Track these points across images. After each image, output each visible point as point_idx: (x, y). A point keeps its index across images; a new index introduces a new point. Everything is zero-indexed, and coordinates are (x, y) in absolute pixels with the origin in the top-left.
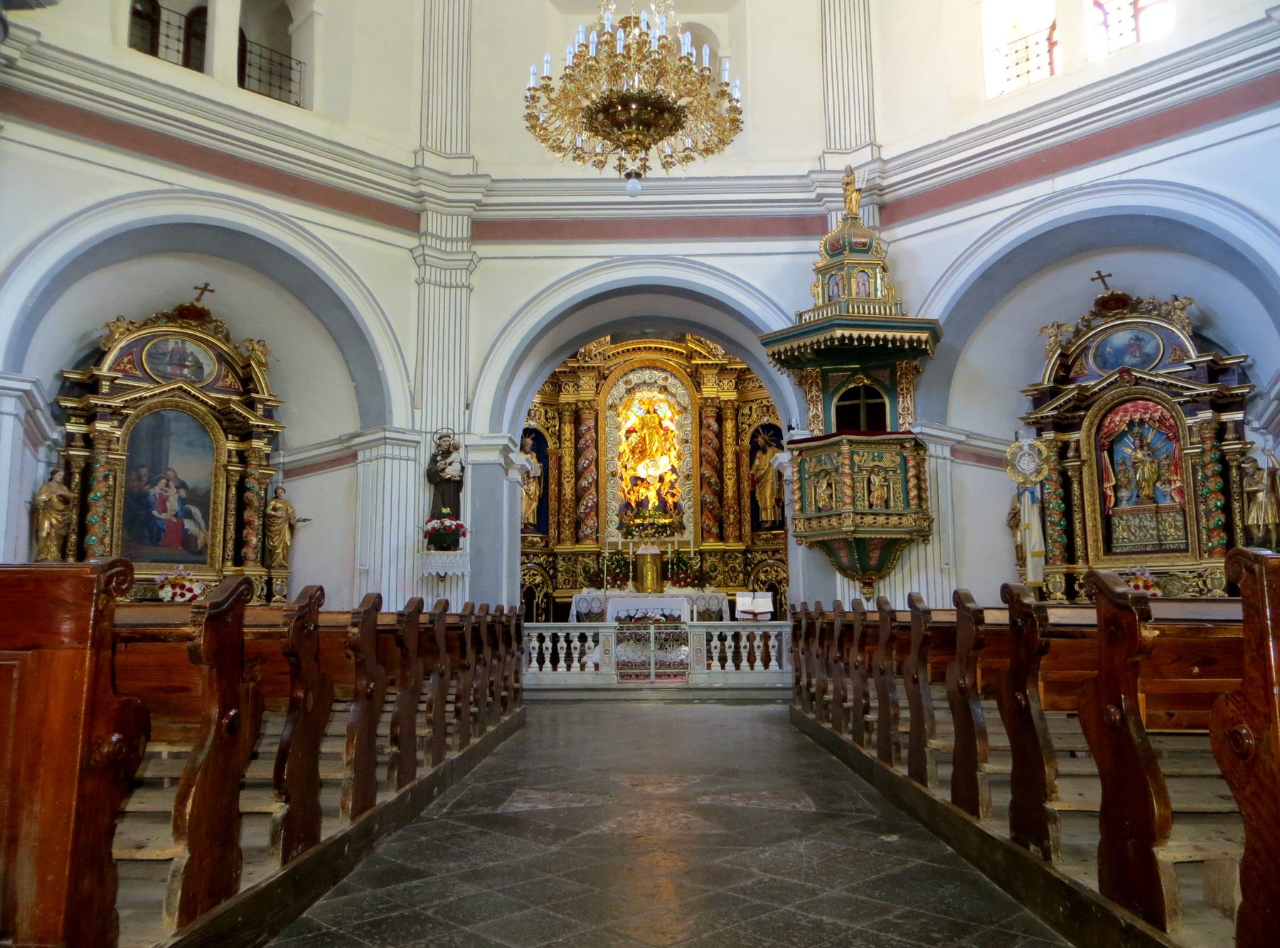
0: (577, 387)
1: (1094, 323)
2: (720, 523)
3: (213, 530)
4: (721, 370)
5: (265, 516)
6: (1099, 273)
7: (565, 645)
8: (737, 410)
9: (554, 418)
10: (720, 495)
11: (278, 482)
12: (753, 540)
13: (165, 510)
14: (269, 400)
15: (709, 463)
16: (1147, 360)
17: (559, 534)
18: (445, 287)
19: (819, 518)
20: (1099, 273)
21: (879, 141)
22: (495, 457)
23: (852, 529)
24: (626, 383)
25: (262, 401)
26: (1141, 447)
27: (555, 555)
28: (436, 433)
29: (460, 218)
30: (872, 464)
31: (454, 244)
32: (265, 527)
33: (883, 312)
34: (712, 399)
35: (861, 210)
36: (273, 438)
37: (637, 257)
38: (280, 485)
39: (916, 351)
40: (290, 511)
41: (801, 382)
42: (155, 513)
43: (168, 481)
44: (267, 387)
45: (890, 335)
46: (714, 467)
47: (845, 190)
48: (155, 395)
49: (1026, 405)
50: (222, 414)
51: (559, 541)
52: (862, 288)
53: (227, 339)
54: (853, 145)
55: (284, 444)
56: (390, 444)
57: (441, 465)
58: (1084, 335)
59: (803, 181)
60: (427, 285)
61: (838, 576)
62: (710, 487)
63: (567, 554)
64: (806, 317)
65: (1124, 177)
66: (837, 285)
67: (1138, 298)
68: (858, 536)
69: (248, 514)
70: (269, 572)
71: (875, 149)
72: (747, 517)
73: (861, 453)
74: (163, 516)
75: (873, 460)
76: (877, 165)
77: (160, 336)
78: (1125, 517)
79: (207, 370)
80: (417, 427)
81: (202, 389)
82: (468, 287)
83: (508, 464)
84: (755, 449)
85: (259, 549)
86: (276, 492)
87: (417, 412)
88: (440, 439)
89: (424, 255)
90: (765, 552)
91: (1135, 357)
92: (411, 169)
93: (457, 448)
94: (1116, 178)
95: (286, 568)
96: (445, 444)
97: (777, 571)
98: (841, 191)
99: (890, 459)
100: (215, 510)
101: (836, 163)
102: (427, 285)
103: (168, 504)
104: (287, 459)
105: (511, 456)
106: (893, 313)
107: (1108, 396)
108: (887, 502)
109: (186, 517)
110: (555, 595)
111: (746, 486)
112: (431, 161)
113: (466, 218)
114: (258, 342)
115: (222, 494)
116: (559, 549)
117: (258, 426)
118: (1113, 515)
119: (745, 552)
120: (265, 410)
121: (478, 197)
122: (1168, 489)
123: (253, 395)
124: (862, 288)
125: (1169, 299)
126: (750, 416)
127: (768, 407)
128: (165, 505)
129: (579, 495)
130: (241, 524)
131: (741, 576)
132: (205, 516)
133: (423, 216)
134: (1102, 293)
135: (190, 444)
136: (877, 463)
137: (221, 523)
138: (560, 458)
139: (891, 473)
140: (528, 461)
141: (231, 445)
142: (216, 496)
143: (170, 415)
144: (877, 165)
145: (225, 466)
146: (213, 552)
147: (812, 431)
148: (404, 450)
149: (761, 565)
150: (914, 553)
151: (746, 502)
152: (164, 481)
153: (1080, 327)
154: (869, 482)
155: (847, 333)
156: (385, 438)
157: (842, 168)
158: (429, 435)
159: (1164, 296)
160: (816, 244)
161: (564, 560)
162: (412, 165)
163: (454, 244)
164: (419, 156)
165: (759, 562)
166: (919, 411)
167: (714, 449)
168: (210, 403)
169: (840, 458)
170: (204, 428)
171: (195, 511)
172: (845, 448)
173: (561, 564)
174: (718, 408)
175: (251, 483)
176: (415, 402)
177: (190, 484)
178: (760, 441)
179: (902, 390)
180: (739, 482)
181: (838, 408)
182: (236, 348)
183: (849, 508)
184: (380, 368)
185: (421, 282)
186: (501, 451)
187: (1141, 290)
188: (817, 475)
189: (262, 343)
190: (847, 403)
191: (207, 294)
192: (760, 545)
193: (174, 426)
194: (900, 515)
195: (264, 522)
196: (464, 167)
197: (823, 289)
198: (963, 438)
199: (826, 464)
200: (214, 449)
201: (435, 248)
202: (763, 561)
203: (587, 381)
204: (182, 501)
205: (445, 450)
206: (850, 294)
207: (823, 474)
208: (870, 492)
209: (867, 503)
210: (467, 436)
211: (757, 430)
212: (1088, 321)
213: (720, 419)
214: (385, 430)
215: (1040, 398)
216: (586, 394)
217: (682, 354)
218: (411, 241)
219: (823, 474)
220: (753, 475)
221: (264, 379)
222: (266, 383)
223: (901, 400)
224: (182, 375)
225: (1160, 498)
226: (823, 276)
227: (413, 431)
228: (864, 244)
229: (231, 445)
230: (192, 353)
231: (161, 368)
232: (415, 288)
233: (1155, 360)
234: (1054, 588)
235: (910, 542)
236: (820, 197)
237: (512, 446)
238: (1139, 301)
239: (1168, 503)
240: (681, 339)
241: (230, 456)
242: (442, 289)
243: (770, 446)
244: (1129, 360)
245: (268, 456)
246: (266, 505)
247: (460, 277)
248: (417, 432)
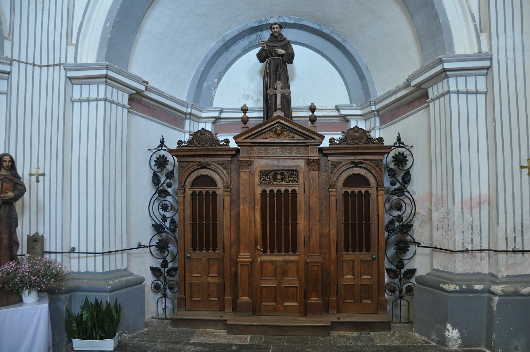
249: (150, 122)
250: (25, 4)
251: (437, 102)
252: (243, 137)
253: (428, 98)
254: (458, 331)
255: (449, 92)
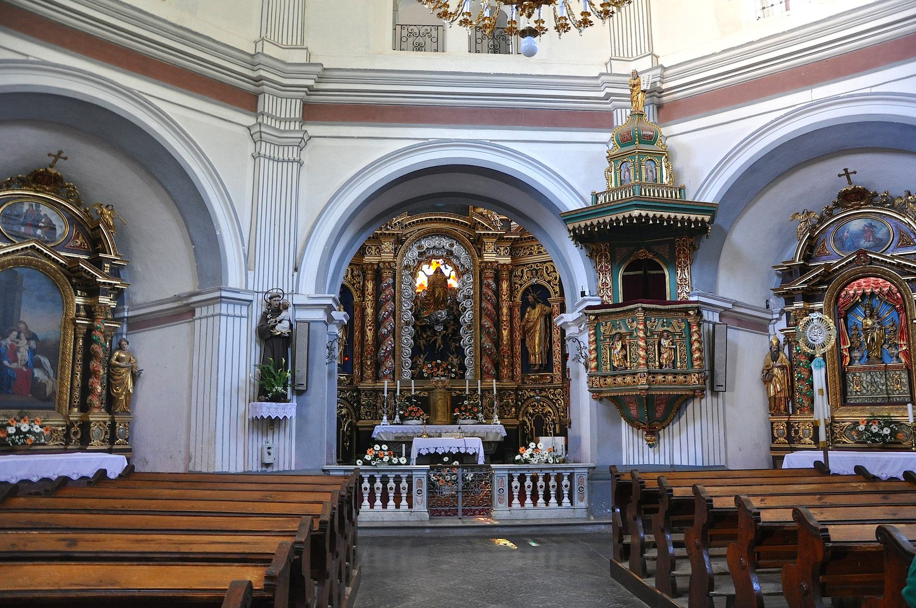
0: (379, 251)
1: (835, 211)
2: (497, 365)
3: (62, 379)
4: (499, 239)
5: (110, 366)
6: (846, 170)
7: (394, 485)
8: (511, 272)
9: (359, 276)
10: (497, 342)
11: (122, 334)
12: (523, 379)
13: (15, 360)
14: (115, 260)
15: (489, 316)
16: (880, 244)
17: (362, 374)
18: (278, 161)
19: (614, 376)
20: (846, 170)
21: (655, 52)
22: (320, 315)
23: (647, 387)
24: (420, 247)
25: (109, 261)
26: (871, 316)
27: (358, 391)
28: (267, 293)
29: (294, 101)
30: (661, 329)
31: (288, 124)
32: (110, 376)
33: (661, 195)
34: (491, 263)
35: (647, 108)
36: (119, 294)
37: (450, 140)
38: (124, 337)
39: (701, 230)
40: (133, 361)
41: (592, 255)
42: (6, 363)
43: (19, 333)
44: (113, 248)
45: (665, 215)
46: (492, 320)
47: (632, 91)
48: (8, 253)
49: (776, 281)
50: (72, 272)
51: (362, 379)
52: (650, 174)
53: (78, 204)
54: (635, 54)
55: (129, 298)
56: (225, 302)
57: (271, 322)
58: (826, 221)
59: (593, 82)
60: (262, 159)
61: (624, 425)
62: (489, 336)
63: (369, 390)
64: (601, 199)
65: (874, 90)
66: (628, 170)
67: (875, 193)
68: (650, 393)
69: (94, 364)
70: (113, 418)
71: (655, 58)
72: (518, 361)
73: (653, 319)
74: (14, 365)
75: (663, 326)
76: (659, 71)
77: (15, 199)
78: (858, 374)
79: (59, 231)
80: (250, 288)
81: (51, 249)
82: (298, 162)
83: (331, 319)
84: (526, 304)
85: (104, 396)
86: (120, 344)
87: (251, 274)
88: (270, 298)
89: (261, 132)
90: (533, 390)
91: (869, 241)
92: (252, 56)
93: (286, 308)
94: (868, 91)
95: (129, 413)
96: (275, 303)
97: (543, 406)
98: (629, 92)
99: (676, 325)
100: (63, 360)
101: (625, 68)
102: (262, 159)
103: (19, 355)
104: (131, 314)
105: (333, 313)
106: (674, 195)
107: (845, 272)
108: (674, 362)
109: (35, 367)
110: (358, 424)
111: (518, 336)
112: (270, 50)
113: (298, 101)
114: (107, 207)
115: (70, 345)
116: (362, 386)
117: (104, 283)
118: (848, 372)
119: (516, 390)
120: (111, 268)
121: (311, 82)
122: (895, 351)
123: (101, 255)
124: (650, 174)
125: (903, 195)
126: (522, 277)
127: (537, 271)
128: (16, 355)
129: (378, 341)
130: (88, 373)
131: (513, 409)
132: (54, 366)
133: (261, 97)
134: (845, 187)
135: (41, 299)
136: (666, 328)
137: (68, 372)
138: (363, 309)
139: (677, 337)
140: (340, 315)
141: (79, 300)
142: (65, 347)
143: (20, 271)
144: (659, 71)
145: (73, 320)
146: (60, 399)
147: (602, 297)
148: (238, 307)
149: (530, 401)
150: (690, 407)
151: (518, 347)
152: (15, 333)
153: (824, 214)
154: (660, 344)
155: (644, 213)
156: (221, 297)
157: (630, 72)
158: (260, 295)
159: (897, 191)
160: (606, 136)
161: (366, 395)
162: (253, 53)
163: (288, 124)
164: (259, 45)
165: (528, 398)
166: (694, 282)
167: (492, 304)
168: (61, 261)
169: (635, 323)
170: (55, 284)
171: (45, 361)
172: (640, 315)
173: (364, 400)
174: (495, 270)
175: (97, 335)
176: (249, 262)
177: (40, 336)
178: (530, 298)
179: (680, 263)
180: (511, 332)
181: (624, 277)
182: (86, 211)
183: (643, 369)
184: (218, 233)
185: (256, 156)
186: (325, 310)
187: (880, 187)
188: (612, 337)
189: (110, 208)
190: (631, 273)
191: (60, 161)
192: (529, 384)
193: (26, 282)
194: (686, 374)
195: (108, 370)
196: (298, 57)
197: (615, 173)
198: (730, 306)
199: (620, 328)
200: (65, 303)
201: (270, 127)
202: (531, 397)
203: (388, 246)
204: (32, 352)
205: (275, 307)
206: (641, 179)
207: (617, 337)
208: (660, 354)
209: (657, 363)
210: (295, 295)
211: (527, 289)
212: (832, 210)
213: (497, 280)
214: (221, 290)
215: (789, 273)
216: (387, 256)
217: (466, 224)
218: (249, 120)
219: (617, 337)
220: (524, 327)
221: (111, 240)
222: (113, 244)
223: (679, 272)
224: (35, 235)
225: (886, 359)
226: (616, 162)
227: (246, 291)
228: (650, 137)
229: (79, 300)
230: (46, 215)
231: (16, 228)
232: (250, 161)
233: (886, 244)
234: (804, 435)
235: (693, 397)
236: (608, 96)
237: (335, 306)
238: (875, 195)
239: (894, 363)
240: (464, 212)
241: (78, 310)
242: (275, 163)
243: (538, 302)
244: (864, 244)
245: (114, 311)
246: (111, 356)
247: (292, 153)
248: (250, 291)
249: (172, 567)
250: (292, 2)
251: (204, 321)
252: (45, 447)
253: (194, 316)
254: (673, 263)
255: (220, 315)
